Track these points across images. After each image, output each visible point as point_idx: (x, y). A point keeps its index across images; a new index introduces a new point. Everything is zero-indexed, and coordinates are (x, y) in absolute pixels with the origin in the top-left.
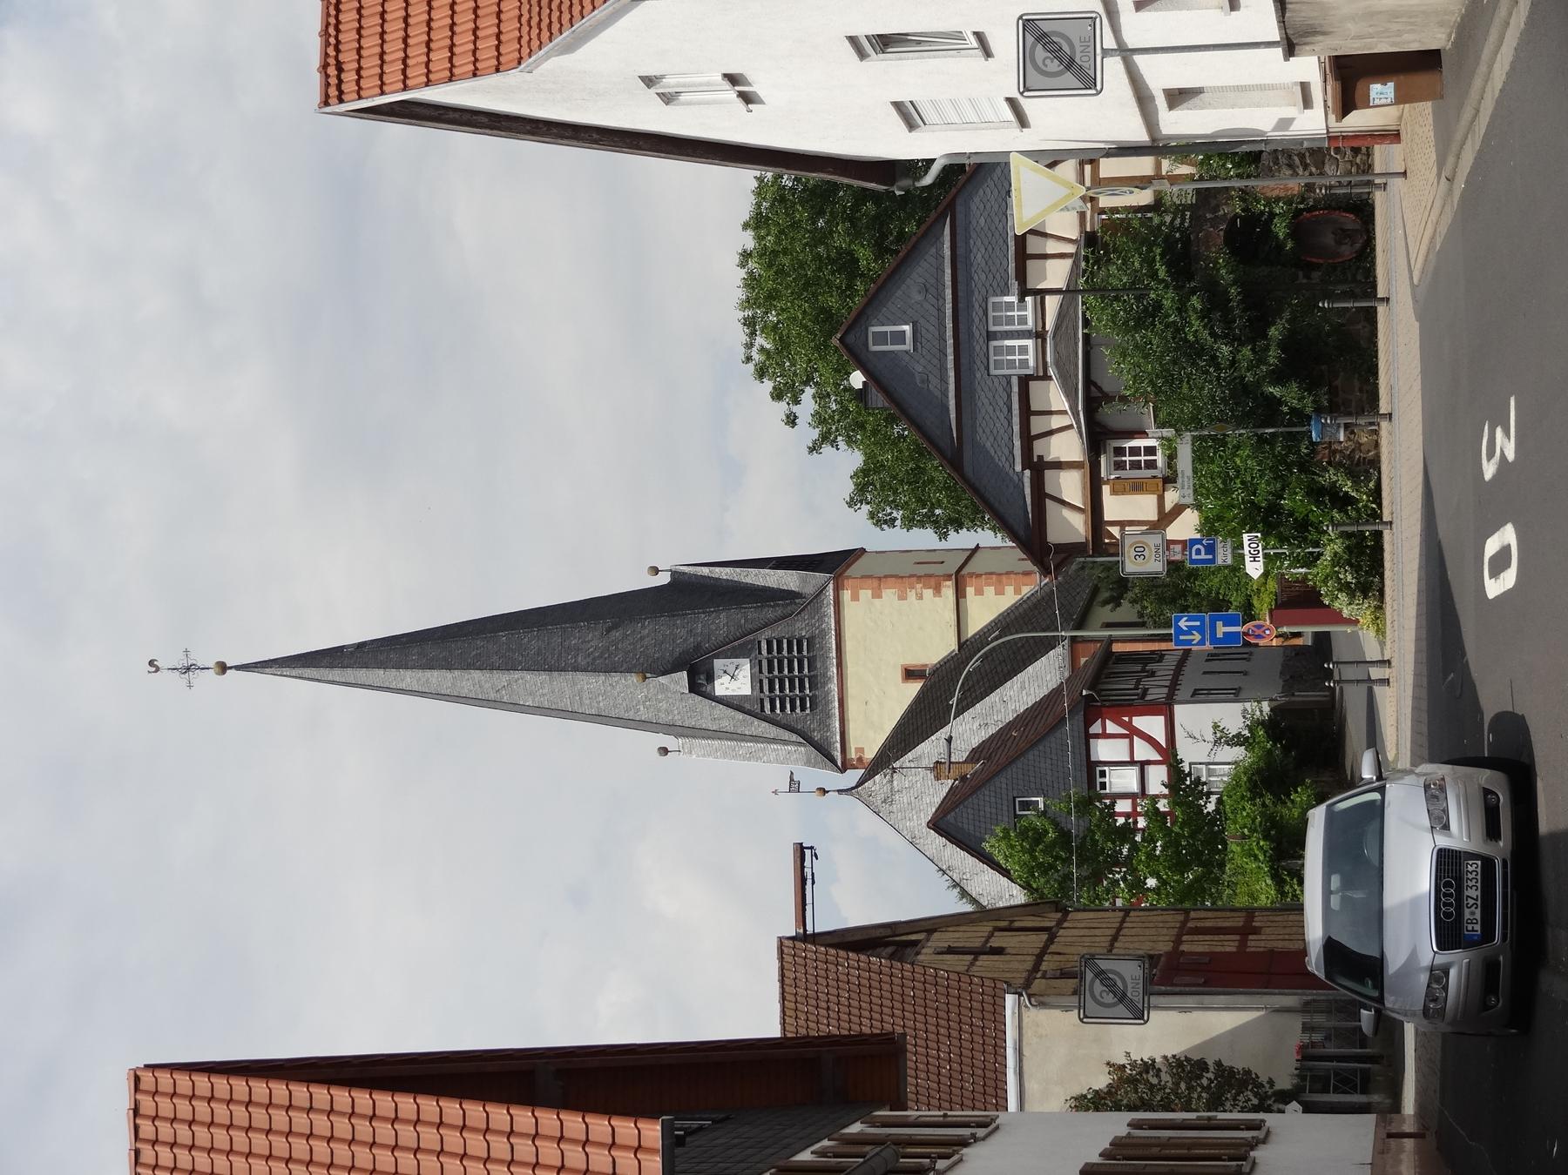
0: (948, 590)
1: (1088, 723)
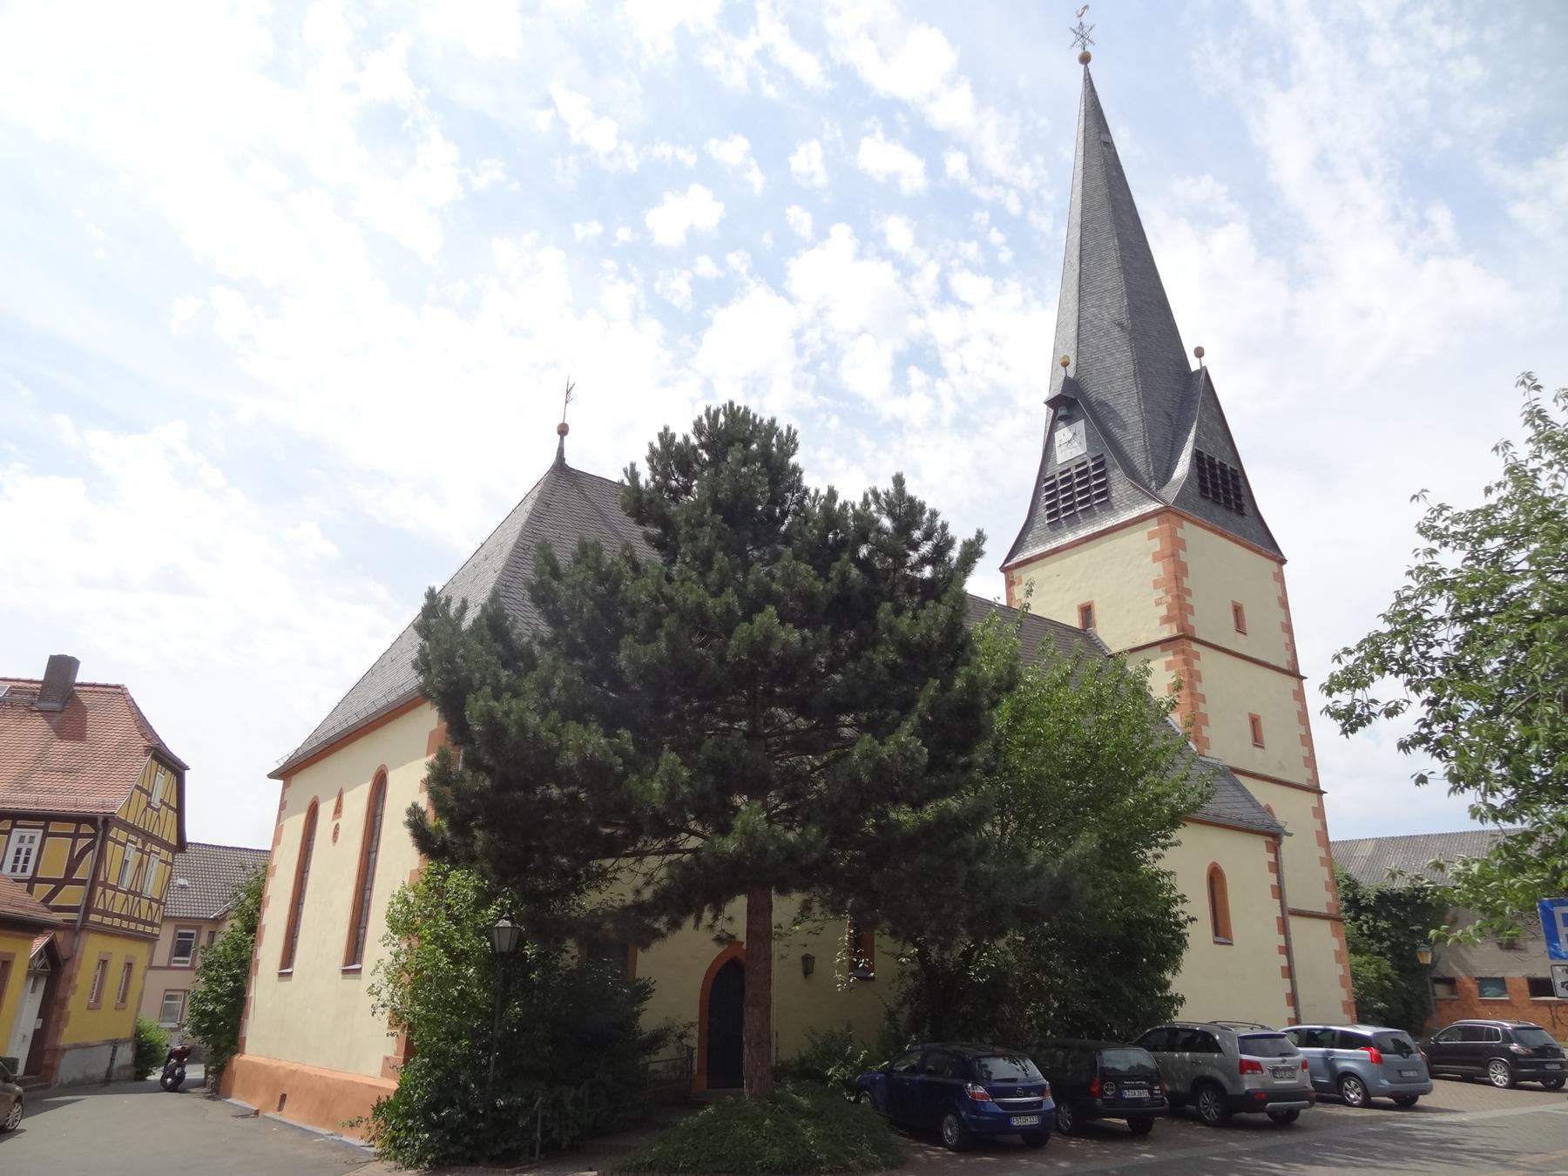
0: (1168, 631)
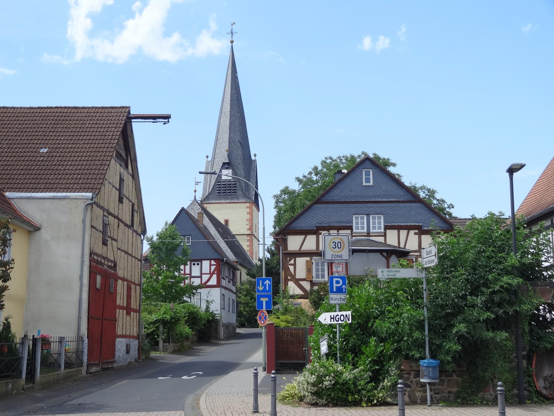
1: (214, 260)
